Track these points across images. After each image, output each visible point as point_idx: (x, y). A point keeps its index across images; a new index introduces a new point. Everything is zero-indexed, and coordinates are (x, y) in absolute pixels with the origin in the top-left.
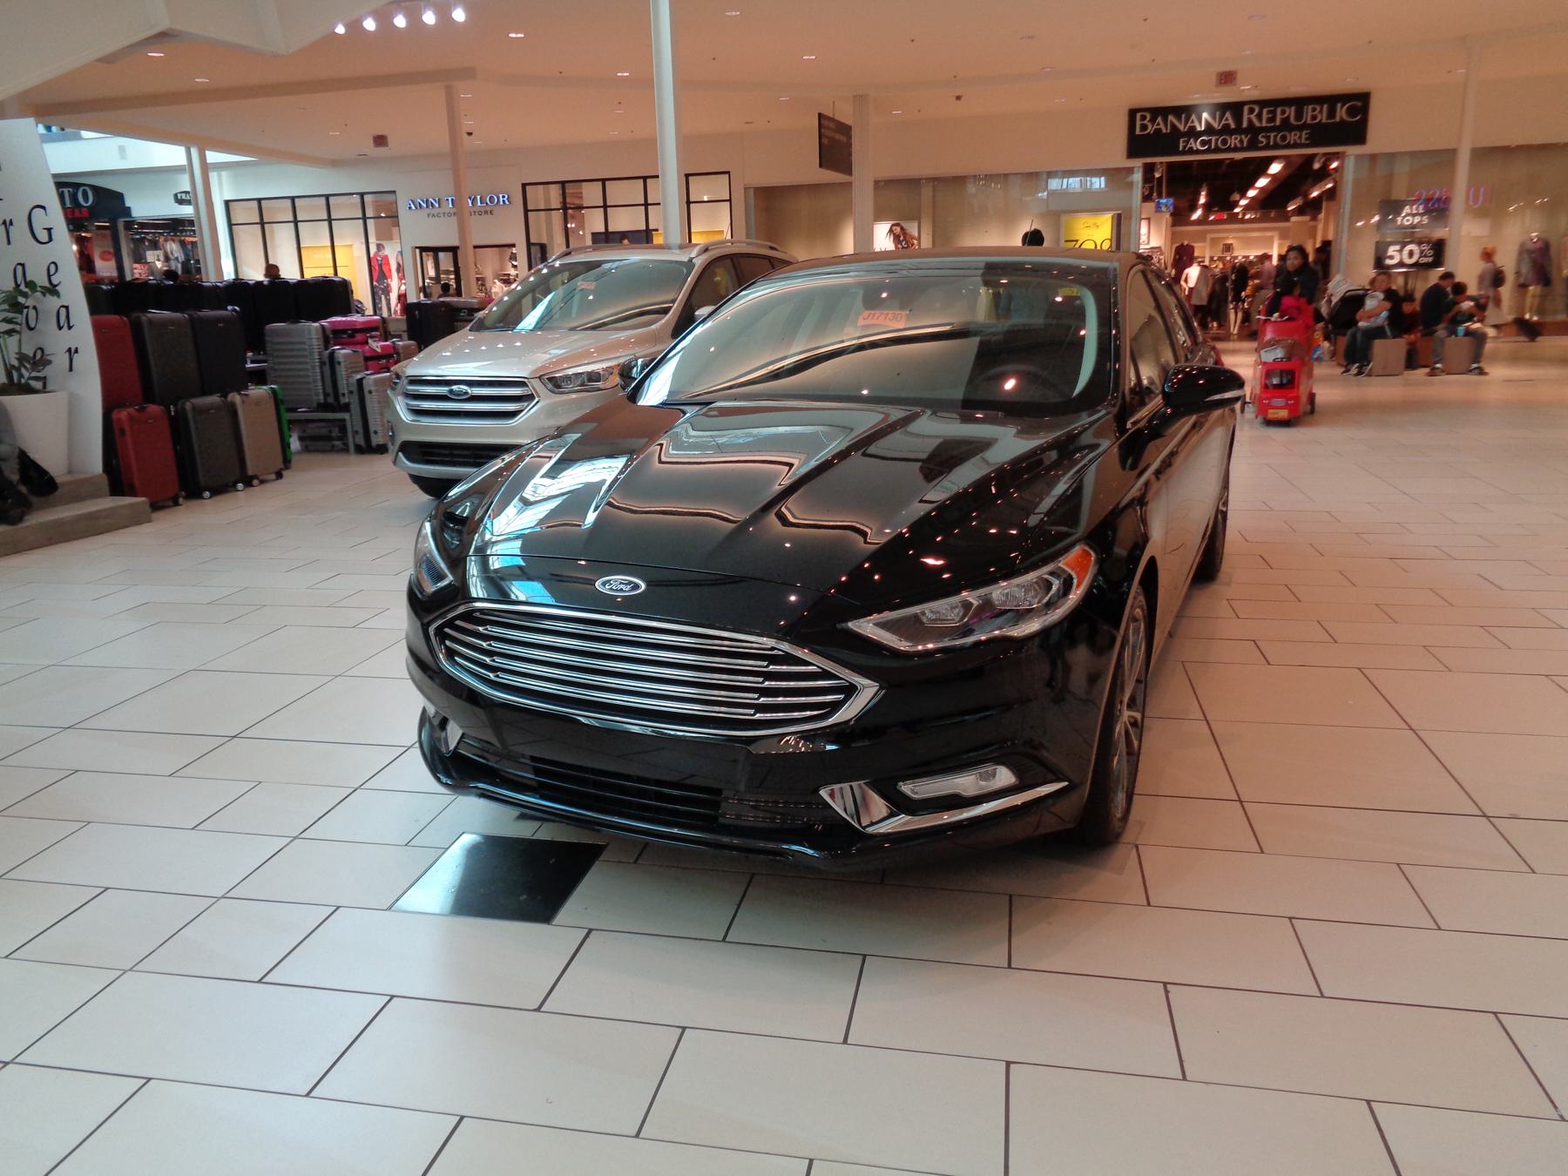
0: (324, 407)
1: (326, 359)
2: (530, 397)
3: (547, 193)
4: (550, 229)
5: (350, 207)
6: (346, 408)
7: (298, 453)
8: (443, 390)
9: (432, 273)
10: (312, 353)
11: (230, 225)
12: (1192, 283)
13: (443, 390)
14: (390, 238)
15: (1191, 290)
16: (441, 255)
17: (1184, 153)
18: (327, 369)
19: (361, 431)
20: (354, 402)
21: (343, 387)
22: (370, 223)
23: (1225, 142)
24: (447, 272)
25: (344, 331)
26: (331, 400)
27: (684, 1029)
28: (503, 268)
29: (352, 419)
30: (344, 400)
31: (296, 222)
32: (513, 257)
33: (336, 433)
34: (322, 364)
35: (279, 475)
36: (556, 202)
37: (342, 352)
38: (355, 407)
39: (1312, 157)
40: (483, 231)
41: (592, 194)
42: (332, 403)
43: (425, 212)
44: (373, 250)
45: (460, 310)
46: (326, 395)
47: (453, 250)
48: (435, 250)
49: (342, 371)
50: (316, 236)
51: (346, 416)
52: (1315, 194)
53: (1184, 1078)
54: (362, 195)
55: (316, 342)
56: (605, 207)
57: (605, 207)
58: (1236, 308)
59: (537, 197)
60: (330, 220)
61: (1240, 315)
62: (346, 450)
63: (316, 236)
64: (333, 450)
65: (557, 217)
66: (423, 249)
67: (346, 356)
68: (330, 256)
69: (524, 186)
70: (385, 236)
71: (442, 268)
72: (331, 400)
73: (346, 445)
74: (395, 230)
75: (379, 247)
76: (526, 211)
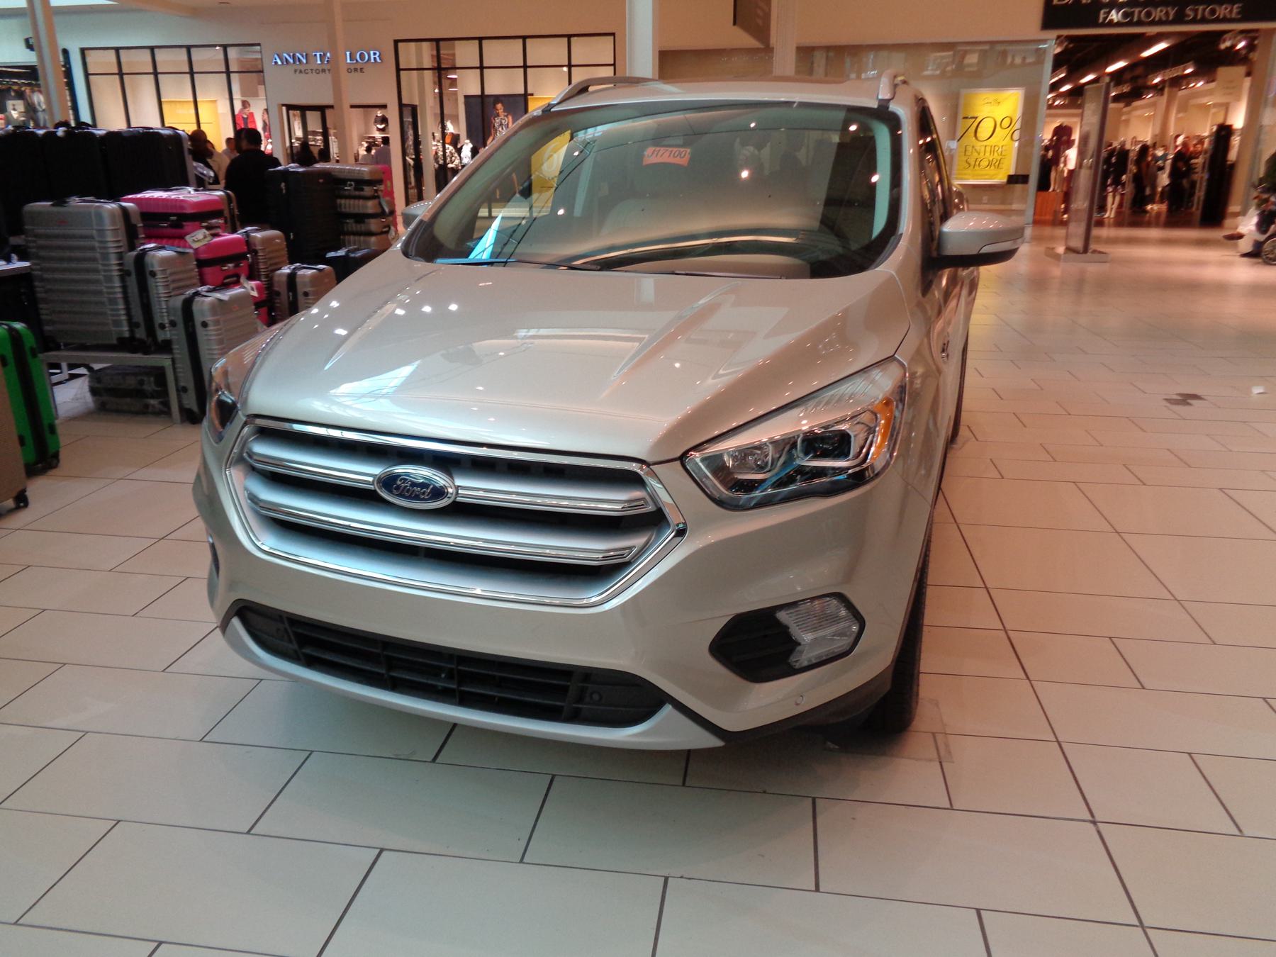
0: (127, 344)
1: (130, 266)
2: (653, 520)
3: (419, 54)
4: (422, 90)
5: (208, 59)
6: (166, 347)
7: (86, 416)
8: (364, 472)
9: (299, 132)
10: (105, 256)
11: (87, 75)
12: (1072, 165)
13: (364, 472)
14: (256, 95)
15: (1071, 172)
16: (308, 113)
17: (1103, 25)
18: (132, 281)
19: (190, 385)
20: (176, 335)
21: (162, 314)
22: (234, 77)
23: (1148, 14)
24: (315, 133)
25: (164, 217)
26: (141, 333)
27: (521, 861)
28: (367, 130)
29: (173, 364)
30: (161, 336)
31: (156, 74)
32: (384, 120)
33: (150, 385)
34: (124, 275)
35: (22, 501)
36: (428, 62)
37: (160, 254)
38: (181, 350)
39: (1220, 35)
40: (357, 90)
41: (465, 54)
42: (145, 338)
43: (291, 69)
44: (238, 106)
45: (343, 181)
46: (133, 325)
47: (322, 109)
48: (303, 109)
49: (158, 288)
50: (177, 90)
51: (163, 360)
52: (1157, 80)
53: (978, 911)
54: (225, 47)
55: (113, 238)
56: (482, 68)
57: (482, 68)
58: (1115, 191)
59: (409, 55)
60: (192, 73)
61: (1118, 198)
62: (165, 411)
63: (177, 90)
64: (144, 412)
65: (429, 76)
66: (290, 107)
67: (165, 261)
68: (193, 111)
69: (396, 42)
70: (249, 92)
71: (310, 129)
72: (141, 333)
73: (166, 404)
74: (261, 88)
75: (245, 104)
76: (398, 70)
